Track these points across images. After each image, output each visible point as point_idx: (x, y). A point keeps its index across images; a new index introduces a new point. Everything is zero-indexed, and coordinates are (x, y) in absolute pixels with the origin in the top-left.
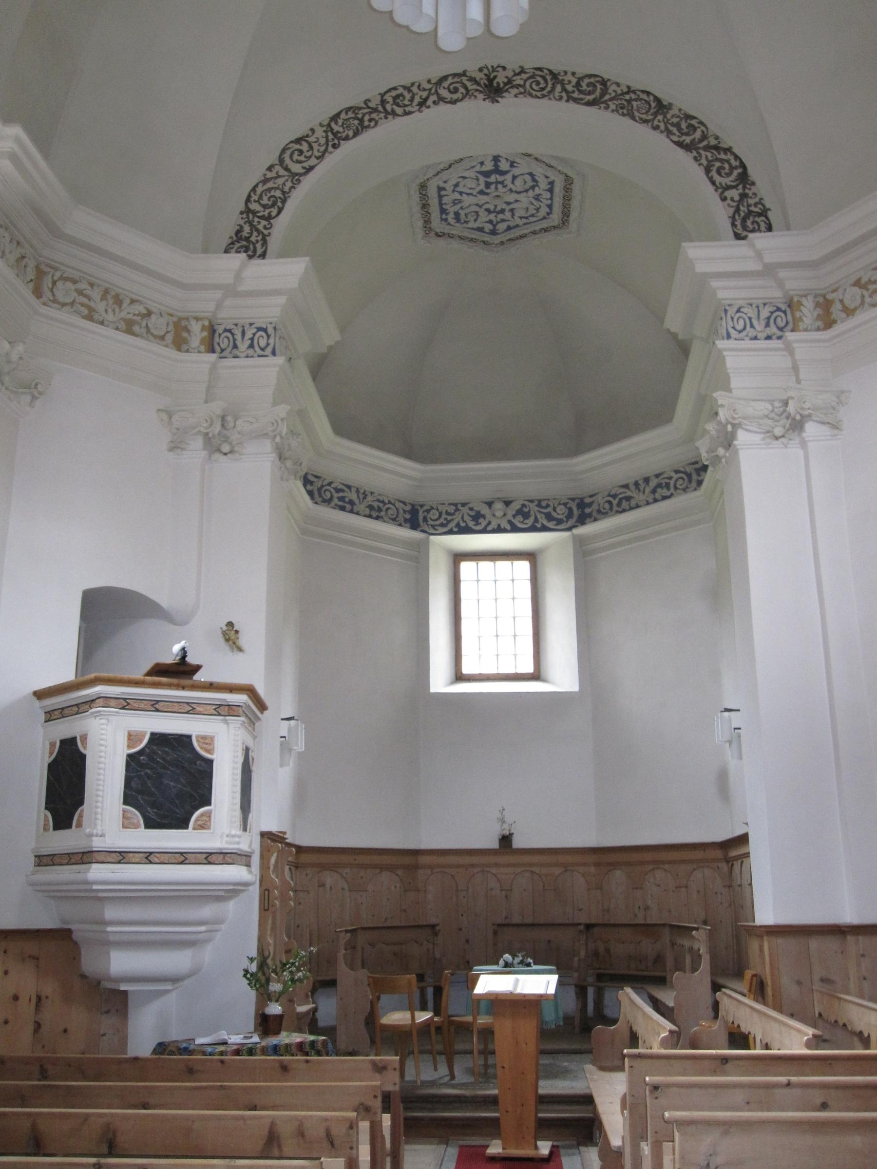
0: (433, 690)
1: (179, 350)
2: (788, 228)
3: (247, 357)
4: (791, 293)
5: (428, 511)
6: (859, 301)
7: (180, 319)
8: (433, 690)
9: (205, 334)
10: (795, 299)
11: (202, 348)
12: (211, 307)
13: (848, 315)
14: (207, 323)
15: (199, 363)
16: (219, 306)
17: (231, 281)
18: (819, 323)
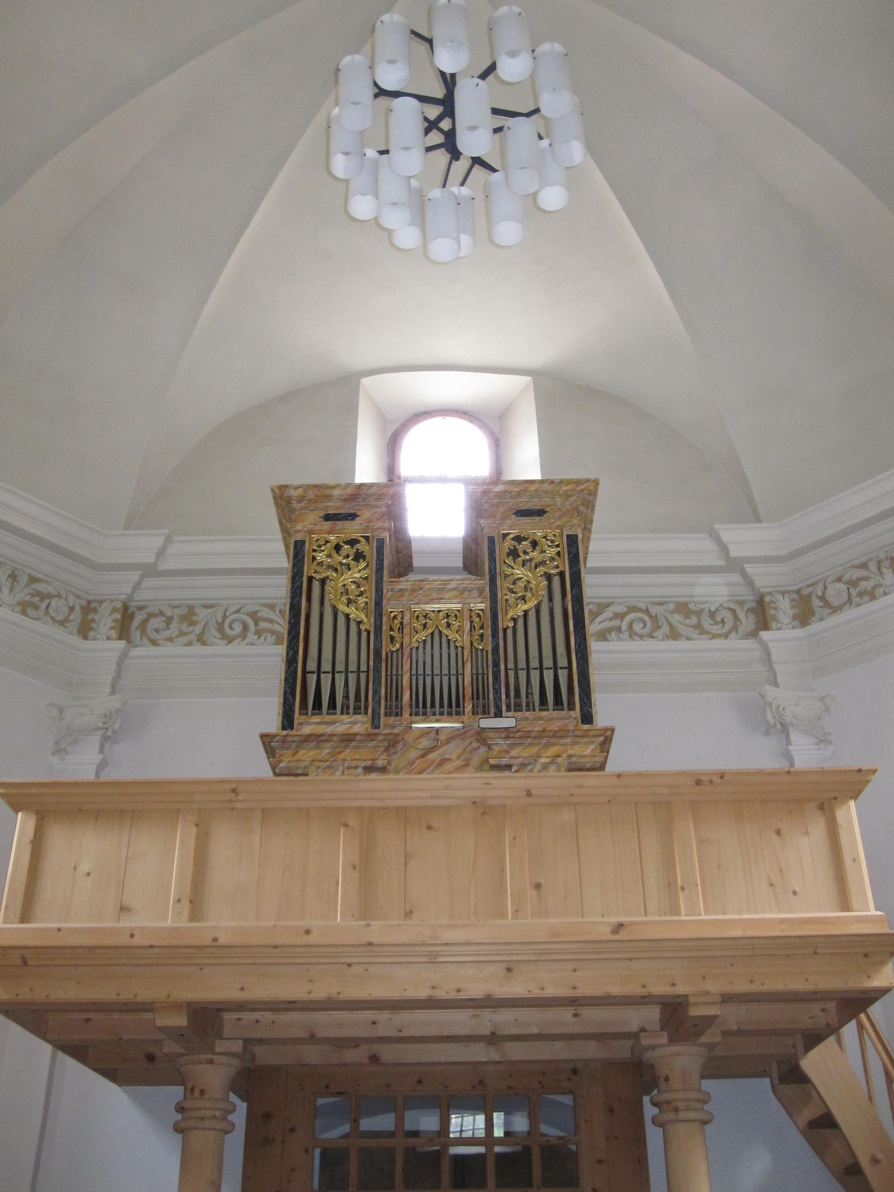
0: (483, 1135)
1: (85, 638)
2: (758, 520)
3: (368, 770)
4: (763, 590)
5: (150, 616)
6: (845, 597)
7: (89, 602)
8: (483, 1135)
9: (118, 616)
10: (767, 599)
11: (113, 634)
12: (128, 589)
13: (630, 637)
14: (119, 605)
15: (106, 648)
16: (137, 586)
17: (152, 560)
18: (796, 623)
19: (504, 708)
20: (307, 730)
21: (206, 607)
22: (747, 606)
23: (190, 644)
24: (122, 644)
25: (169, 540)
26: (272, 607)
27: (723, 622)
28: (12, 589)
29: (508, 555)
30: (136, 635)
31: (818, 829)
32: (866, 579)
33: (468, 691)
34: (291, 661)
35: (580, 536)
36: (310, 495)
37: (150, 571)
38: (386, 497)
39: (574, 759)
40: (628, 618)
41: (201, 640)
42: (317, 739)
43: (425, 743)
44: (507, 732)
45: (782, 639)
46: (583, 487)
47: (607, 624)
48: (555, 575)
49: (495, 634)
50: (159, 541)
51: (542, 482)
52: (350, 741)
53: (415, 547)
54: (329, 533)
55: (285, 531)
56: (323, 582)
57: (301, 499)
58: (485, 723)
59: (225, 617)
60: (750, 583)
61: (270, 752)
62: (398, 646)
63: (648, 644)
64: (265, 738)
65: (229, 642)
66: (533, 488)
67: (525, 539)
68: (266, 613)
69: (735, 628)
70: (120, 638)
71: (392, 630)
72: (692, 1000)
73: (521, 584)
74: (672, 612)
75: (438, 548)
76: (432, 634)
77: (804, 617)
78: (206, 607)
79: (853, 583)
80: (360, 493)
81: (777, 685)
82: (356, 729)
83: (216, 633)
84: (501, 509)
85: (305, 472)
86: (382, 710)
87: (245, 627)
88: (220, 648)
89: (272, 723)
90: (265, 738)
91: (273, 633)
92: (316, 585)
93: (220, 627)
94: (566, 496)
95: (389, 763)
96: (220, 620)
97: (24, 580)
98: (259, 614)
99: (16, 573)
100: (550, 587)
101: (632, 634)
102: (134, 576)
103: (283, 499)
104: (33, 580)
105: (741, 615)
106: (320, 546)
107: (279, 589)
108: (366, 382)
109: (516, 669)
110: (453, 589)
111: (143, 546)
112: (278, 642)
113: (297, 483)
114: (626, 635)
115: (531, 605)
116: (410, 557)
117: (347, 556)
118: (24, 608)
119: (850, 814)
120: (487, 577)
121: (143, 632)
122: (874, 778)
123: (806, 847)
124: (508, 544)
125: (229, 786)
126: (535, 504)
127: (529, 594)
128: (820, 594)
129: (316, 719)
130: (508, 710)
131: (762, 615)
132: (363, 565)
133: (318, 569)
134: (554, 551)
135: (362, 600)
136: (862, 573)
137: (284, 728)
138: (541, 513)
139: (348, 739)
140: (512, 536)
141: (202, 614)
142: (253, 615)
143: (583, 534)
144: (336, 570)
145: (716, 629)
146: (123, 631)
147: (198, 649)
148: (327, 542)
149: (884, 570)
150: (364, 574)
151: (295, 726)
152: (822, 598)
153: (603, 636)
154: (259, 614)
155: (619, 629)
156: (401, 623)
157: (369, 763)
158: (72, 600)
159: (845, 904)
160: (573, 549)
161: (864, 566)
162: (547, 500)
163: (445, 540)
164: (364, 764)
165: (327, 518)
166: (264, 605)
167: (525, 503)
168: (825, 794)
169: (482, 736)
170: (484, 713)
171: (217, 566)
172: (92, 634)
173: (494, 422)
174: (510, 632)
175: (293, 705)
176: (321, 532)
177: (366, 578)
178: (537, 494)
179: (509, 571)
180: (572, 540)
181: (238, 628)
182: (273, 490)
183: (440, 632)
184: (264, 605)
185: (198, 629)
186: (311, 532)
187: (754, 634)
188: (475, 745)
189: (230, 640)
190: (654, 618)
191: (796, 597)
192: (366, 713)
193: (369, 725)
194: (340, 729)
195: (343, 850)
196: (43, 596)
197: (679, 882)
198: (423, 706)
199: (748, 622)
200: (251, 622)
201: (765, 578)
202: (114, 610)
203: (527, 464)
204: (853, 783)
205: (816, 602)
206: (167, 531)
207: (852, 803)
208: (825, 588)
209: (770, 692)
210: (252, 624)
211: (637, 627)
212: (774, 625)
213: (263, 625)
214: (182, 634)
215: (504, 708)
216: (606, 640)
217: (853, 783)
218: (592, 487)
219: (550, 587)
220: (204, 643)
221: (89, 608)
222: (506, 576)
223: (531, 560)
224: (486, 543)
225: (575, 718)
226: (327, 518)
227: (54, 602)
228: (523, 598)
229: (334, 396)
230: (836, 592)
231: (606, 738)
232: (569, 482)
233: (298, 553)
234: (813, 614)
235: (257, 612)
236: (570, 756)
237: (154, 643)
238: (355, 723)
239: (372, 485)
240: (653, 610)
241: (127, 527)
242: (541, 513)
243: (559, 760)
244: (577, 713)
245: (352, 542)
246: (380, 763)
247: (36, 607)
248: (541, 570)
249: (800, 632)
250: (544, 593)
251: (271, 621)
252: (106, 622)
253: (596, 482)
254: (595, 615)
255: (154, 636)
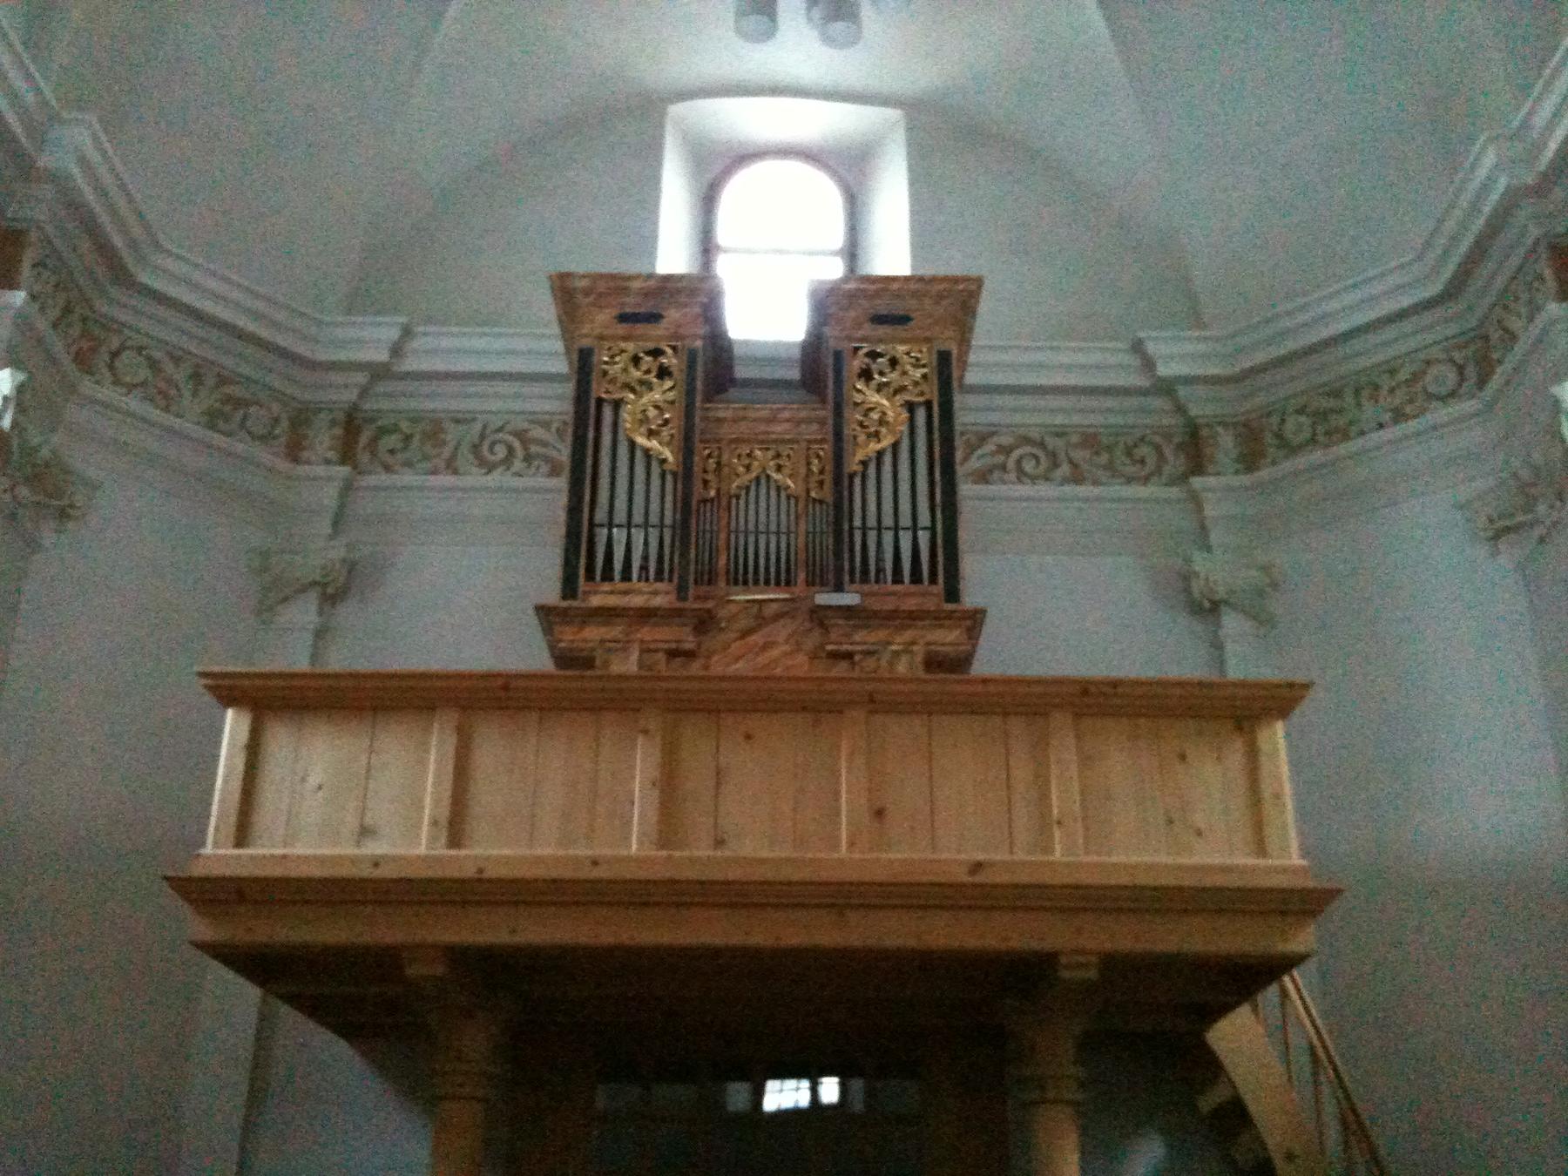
1: (296, 460)
5: (383, 431)
9: (338, 431)
10: (1205, 432)
14: (341, 416)
16: (364, 392)
19: (847, 578)
20: (596, 601)
21: (458, 421)
22: (1176, 440)
23: (434, 472)
24: (344, 471)
25: (407, 332)
26: (546, 425)
27: (1142, 462)
28: (195, 394)
29: (860, 376)
30: (364, 458)
31: (1235, 756)
32: (1340, 411)
33: (802, 556)
34: (574, 510)
35: (955, 352)
36: (602, 286)
37: (379, 372)
38: (697, 294)
39: (933, 647)
40: (1016, 454)
41: (452, 467)
42: (608, 615)
43: (744, 623)
44: (847, 611)
45: (1220, 489)
46: (961, 287)
47: (989, 461)
48: (920, 404)
49: (837, 481)
50: (394, 334)
51: (907, 279)
52: (649, 616)
53: (737, 351)
54: (625, 339)
55: (568, 334)
56: (617, 405)
57: (587, 292)
58: (824, 598)
59: (482, 437)
60: (1180, 409)
61: (548, 629)
62: (713, 493)
63: (1044, 489)
64: (543, 611)
65: (489, 472)
66: (895, 286)
67: (880, 355)
68: (538, 432)
69: (1158, 471)
70: (343, 462)
71: (705, 471)
72: (1063, 960)
73: (875, 416)
74: (1076, 446)
75: (769, 356)
76: (758, 479)
77: (1250, 460)
78: (458, 421)
79: (1322, 415)
80: (669, 287)
81: (1209, 549)
82: (658, 601)
83: (471, 457)
84: (853, 314)
85: (589, 259)
86: (691, 578)
87: (511, 450)
88: (474, 478)
89: (551, 594)
90: (543, 611)
91: (547, 459)
92: (607, 412)
93: (476, 448)
94: (940, 297)
95: (699, 645)
96: (476, 440)
97: (210, 381)
98: (530, 434)
99: (202, 371)
100: (912, 420)
101: (1021, 475)
102: (361, 378)
103: (566, 291)
104: (222, 381)
105: (1168, 452)
106: (612, 357)
107: (557, 403)
108: (676, 110)
109: (864, 528)
110: (788, 421)
111: (371, 339)
112: (554, 472)
113: (581, 270)
114: (1012, 476)
115: (886, 442)
116: (730, 367)
117: (648, 372)
118: (212, 419)
119: (1276, 737)
120: (830, 406)
121: (374, 454)
122: (1312, 693)
123: (1211, 776)
124: (857, 363)
125: (500, 682)
126: (898, 308)
127: (884, 430)
128: (1275, 428)
129: (606, 587)
130: (852, 581)
131: (1194, 450)
132: (668, 384)
133: (611, 388)
134: (918, 373)
135: (665, 432)
136: (1332, 403)
137: (564, 598)
138: (904, 320)
139: (646, 615)
140: (865, 350)
141: (452, 433)
142: (520, 435)
143: (960, 350)
144: (633, 390)
145: (1131, 470)
146: (347, 454)
147: (446, 480)
148: (623, 351)
149: (1364, 401)
150: (671, 395)
151: (580, 594)
152: (1279, 436)
153: (983, 477)
154: (530, 434)
155: (1003, 468)
156: (718, 463)
157: (674, 646)
158: (276, 407)
159: (1261, 849)
160: (945, 369)
161: (1337, 394)
162: (913, 303)
163: (777, 345)
164: (666, 646)
165: (623, 318)
166: (532, 422)
167: (882, 306)
168: (1242, 710)
169: (820, 616)
170: (822, 585)
171: (474, 368)
172: (305, 454)
173: (849, 168)
174: (857, 481)
175: (577, 567)
176: (615, 338)
177: (672, 402)
178: (898, 295)
179: (858, 398)
180: (944, 358)
181: (501, 452)
182: (550, 278)
183: (768, 477)
184: (532, 422)
185: (447, 452)
186: (601, 338)
187: (1182, 479)
188: (807, 625)
189: (490, 468)
190: (1053, 456)
191: (1241, 429)
192: (670, 580)
193: (672, 597)
194: (637, 601)
195: (642, 765)
196: (239, 403)
197: (1055, 811)
198: (740, 578)
199: (1175, 463)
200: (517, 444)
201: (1201, 407)
202: (333, 423)
203: (891, 256)
204: (1280, 700)
205: (1269, 438)
206: (403, 319)
207: (1280, 727)
208: (1283, 421)
209: (1200, 563)
210: (520, 447)
211: (1029, 466)
212: (1211, 469)
213: (534, 449)
214: (426, 458)
215: (847, 578)
216: (987, 482)
217: (1280, 700)
218: (973, 287)
219: (912, 420)
220: (456, 472)
221: (301, 419)
222: (856, 404)
223: (887, 384)
224: (830, 361)
225: (937, 595)
226: (623, 318)
227: (252, 409)
228: (877, 435)
229: (624, 126)
230: (1297, 427)
231: (975, 619)
232: (945, 279)
233: (584, 364)
234: (1263, 455)
235: (526, 431)
236: (928, 644)
237: (388, 469)
238: (655, 593)
239: (681, 278)
240: (1051, 442)
241: (349, 312)
242: (904, 320)
243: (915, 648)
244: (940, 587)
245: (656, 353)
246: (688, 646)
247: (227, 420)
248: (899, 399)
249: (1246, 479)
250: (904, 428)
251: (545, 444)
252: (323, 440)
253: (979, 282)
254: (971, 449)
255: (389, 460)
